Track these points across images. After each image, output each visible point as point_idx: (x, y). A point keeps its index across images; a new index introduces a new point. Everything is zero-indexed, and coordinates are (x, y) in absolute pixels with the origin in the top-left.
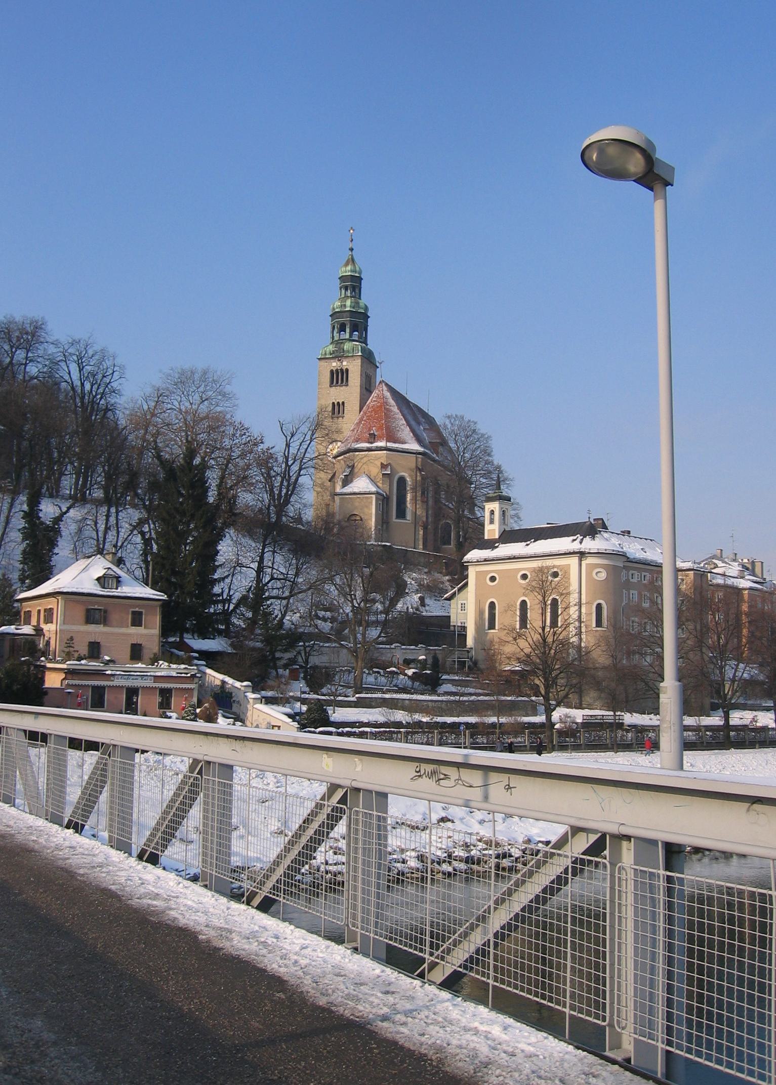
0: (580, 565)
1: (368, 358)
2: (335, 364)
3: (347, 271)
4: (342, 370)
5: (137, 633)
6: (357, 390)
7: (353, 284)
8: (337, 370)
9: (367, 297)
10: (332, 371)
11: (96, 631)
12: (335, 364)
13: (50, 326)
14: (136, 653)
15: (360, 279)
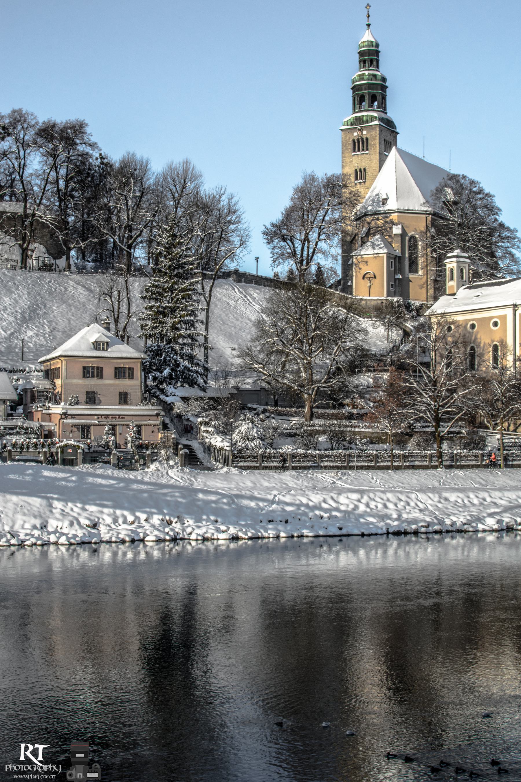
0: (515, 315)
4: (362, 139)
5: (125, 384)
7: (370, 56)
9: (387, 68)
10: (354, 141)
11: (92, 383)
13: (88, 130)
14: (124, 398)
15: (377, 53)
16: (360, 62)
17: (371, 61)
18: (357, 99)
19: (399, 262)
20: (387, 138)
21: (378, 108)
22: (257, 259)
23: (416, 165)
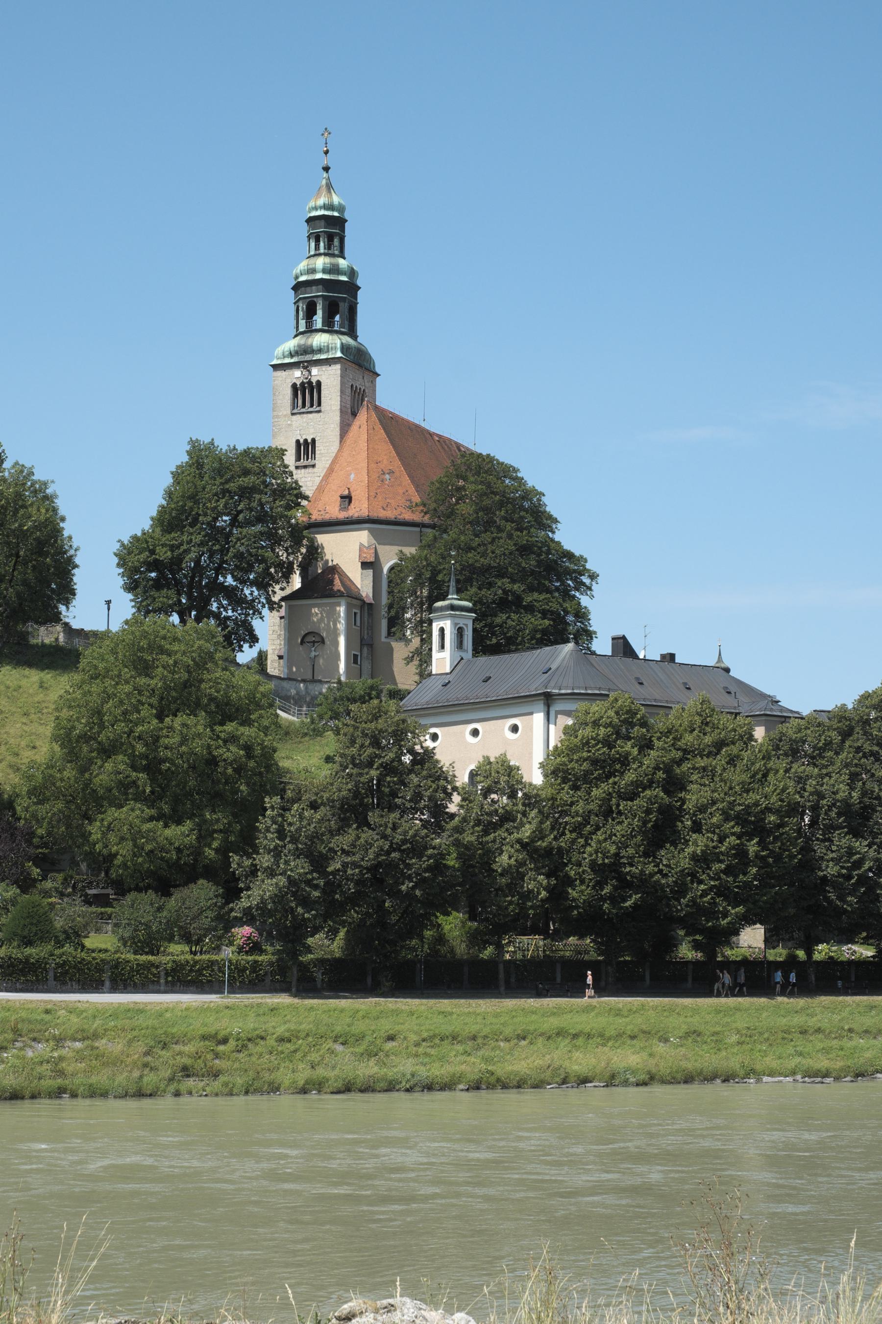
1: (358, 362)
2: (297, 375)
3: (317, 204)
4: (310, 383)
6: (336, 418)
7: (329, 231)
8: (303, 384)
10: (294, 386)
12: (297, 375)
16: (309, 237)
17: (330, 238)
18: (302, 306)
19: (370, 615)
20: (358, 384)
21: (341, 327)
22: (108, 603)
23: (399, 432)
